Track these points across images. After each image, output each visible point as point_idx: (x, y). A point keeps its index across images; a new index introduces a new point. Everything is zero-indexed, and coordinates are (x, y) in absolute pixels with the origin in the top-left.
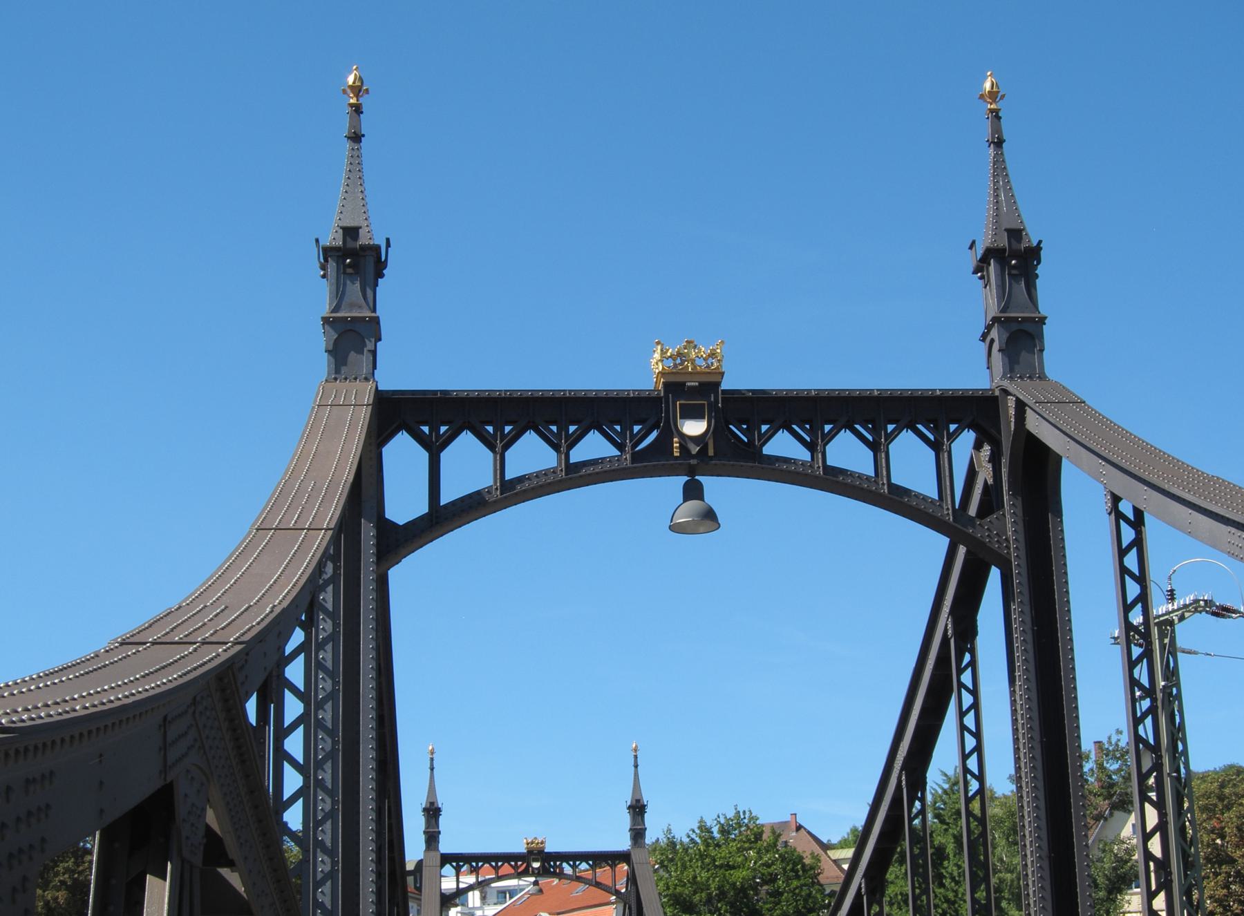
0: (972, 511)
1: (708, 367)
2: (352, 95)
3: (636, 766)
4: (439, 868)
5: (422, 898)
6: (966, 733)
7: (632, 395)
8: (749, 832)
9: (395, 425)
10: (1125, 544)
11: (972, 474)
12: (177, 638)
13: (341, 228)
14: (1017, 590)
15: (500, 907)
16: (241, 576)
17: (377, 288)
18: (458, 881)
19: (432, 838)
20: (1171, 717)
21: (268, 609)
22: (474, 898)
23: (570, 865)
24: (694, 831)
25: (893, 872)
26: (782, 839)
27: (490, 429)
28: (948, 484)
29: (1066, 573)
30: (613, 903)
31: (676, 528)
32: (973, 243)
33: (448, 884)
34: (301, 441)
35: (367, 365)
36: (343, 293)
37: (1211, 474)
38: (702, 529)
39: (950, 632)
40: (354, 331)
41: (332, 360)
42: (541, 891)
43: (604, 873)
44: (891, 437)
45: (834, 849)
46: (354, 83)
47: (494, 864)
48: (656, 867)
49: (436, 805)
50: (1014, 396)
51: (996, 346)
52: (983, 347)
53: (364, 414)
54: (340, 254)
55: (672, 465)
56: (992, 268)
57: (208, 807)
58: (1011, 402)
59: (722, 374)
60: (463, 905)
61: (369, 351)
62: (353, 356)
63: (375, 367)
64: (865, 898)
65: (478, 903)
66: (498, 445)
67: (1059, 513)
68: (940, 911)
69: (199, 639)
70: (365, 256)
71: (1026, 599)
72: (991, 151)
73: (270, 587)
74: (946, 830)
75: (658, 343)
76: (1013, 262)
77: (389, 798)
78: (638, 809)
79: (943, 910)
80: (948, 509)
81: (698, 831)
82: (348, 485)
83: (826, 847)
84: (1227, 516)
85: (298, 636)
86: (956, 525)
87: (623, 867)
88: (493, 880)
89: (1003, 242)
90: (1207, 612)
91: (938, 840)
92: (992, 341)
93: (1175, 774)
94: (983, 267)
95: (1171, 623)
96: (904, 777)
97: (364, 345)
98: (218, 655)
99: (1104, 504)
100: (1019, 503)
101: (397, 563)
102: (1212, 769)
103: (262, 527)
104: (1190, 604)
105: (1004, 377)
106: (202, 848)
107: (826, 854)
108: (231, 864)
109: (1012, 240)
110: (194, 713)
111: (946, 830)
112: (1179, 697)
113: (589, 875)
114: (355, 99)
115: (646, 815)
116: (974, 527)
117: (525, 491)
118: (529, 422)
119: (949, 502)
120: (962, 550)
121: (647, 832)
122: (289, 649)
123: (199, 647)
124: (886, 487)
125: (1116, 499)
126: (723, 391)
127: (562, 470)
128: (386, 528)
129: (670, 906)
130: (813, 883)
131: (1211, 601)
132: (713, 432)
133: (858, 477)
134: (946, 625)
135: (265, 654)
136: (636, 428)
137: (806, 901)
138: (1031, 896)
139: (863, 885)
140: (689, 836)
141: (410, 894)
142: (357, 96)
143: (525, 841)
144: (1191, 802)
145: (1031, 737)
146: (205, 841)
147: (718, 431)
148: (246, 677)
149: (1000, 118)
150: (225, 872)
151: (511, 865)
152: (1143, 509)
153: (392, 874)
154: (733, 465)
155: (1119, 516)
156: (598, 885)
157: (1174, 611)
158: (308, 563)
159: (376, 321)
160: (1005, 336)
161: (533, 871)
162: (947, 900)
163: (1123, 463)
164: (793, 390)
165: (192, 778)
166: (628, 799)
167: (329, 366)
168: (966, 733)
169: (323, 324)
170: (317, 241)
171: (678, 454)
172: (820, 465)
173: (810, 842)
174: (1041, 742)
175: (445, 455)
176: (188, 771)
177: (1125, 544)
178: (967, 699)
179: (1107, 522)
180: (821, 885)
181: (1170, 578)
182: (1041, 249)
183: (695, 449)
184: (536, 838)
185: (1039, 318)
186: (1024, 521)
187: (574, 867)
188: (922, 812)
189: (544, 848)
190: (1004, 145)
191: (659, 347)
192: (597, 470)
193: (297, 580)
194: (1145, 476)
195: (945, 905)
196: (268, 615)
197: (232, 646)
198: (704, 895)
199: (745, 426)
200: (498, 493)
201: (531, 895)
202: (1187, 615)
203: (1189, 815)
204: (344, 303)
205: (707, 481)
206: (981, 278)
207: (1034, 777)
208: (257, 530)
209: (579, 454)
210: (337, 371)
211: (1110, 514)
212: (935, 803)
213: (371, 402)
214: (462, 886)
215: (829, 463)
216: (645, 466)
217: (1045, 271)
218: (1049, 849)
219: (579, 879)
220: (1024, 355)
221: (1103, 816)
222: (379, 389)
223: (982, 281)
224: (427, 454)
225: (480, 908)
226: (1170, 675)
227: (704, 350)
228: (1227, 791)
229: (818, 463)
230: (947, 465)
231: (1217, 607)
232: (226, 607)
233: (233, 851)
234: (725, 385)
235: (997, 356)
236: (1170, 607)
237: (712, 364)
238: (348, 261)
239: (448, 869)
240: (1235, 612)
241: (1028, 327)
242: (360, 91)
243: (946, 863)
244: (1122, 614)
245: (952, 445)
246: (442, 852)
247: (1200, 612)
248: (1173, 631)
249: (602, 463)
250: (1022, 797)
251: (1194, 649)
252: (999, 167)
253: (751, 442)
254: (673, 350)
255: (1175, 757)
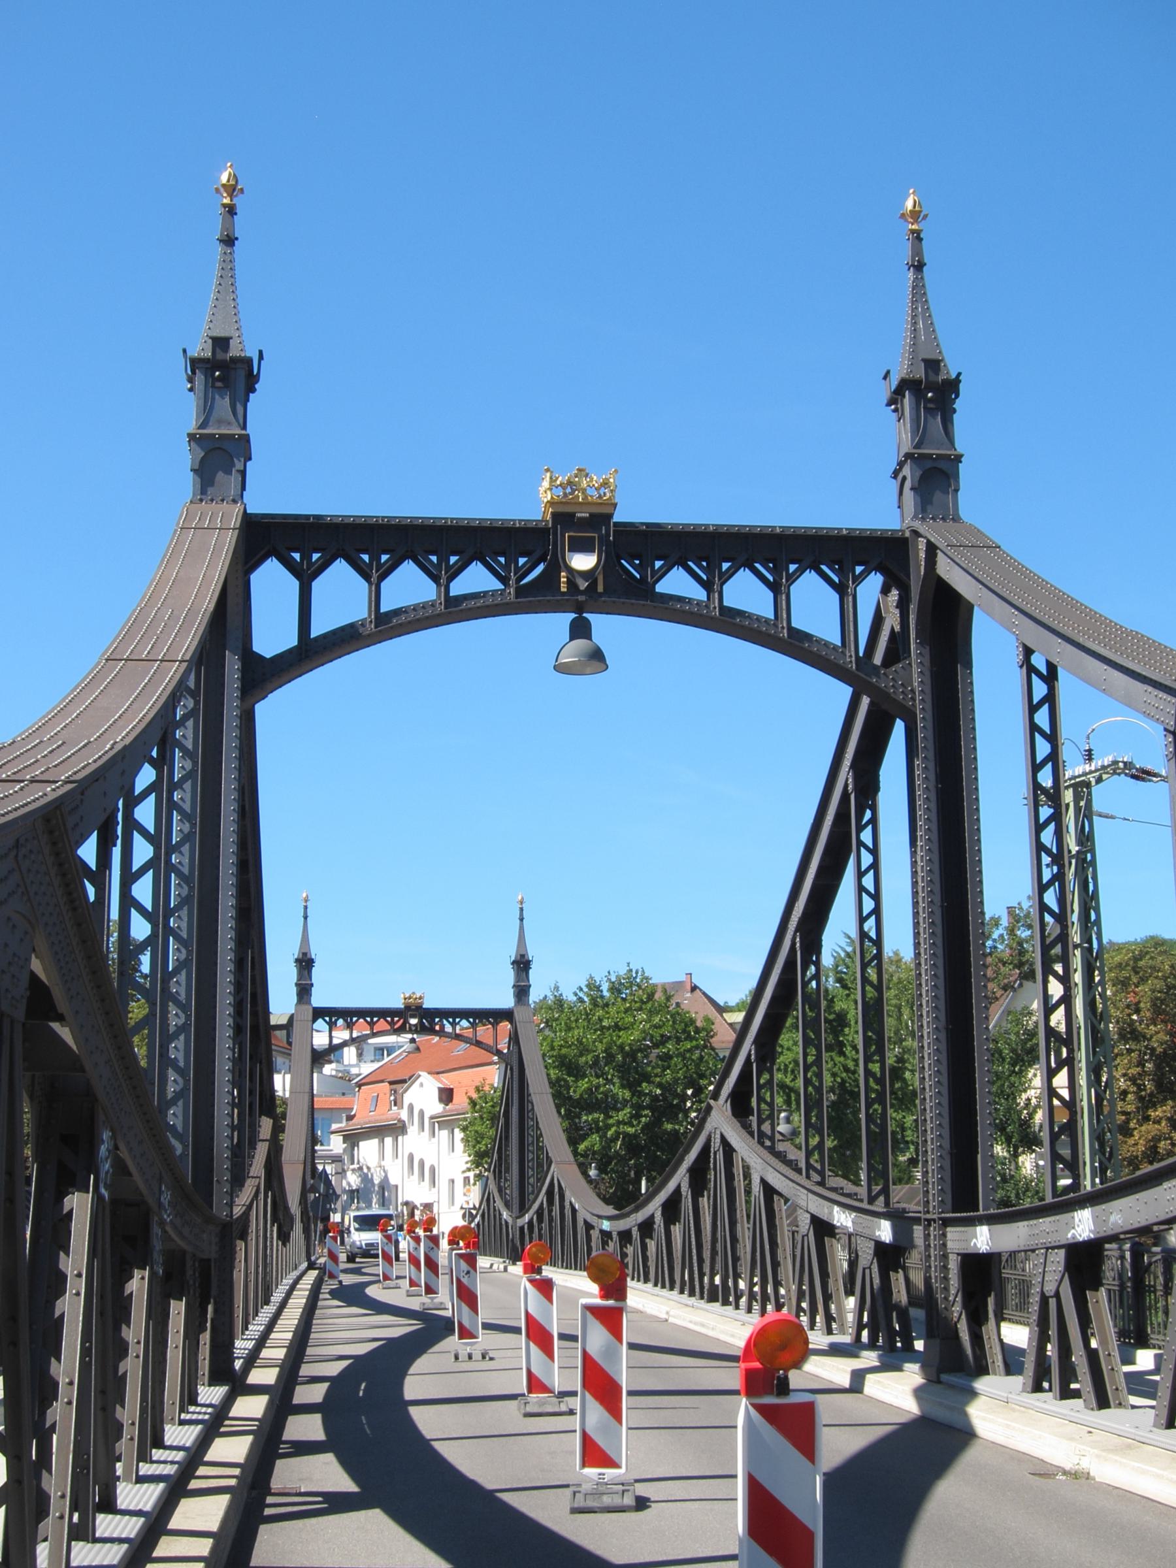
0: (878, 660)
1: (600, 497)
2: (225, 195)
3: (522, 919)
4: (310, 1023)
5: (293, 1052)
6: (864, 894)
7: (518, 525)
8: (641, 991)
9: (262, 552)
10: (1036, 699)
11: (878, 620)
12: (4, 776)
13: (211, 338)
14: (921, 745)
15: (376, 1065)
16: (85, 709)
17: (249, 404)
18: (331, 1037)
19: (304, 991)
20: (1084, 885)
21: (108, 746)
22: (350, 1054)
23: (449, 1022)
24: (581, 989)
25: (785, 1039)
26: (673, 1002)
27: (366, 557)
28: (852, 629)
29: (974, 729)
30: (496, 1063)
31: (560, 668)
32: (888, 372)
33: (320, 1040)
34: (160, 566)
35: (235, 486)
36: (212, 407)
37: (1130, 628)
38: (588, 670)
39: (850, 787)
40: (224, 450)
41: (198, 480)
42: (418, 1049)
43: (484, 1032)
44: (792, 579)
45: (731, 1011)
46: (228, 181)
47: (369, 1019)
48: (542, 1026)
49: (308, 956)
50: (925, 537)
51: (908, 484)
52: (894, 485)
53: (230, 539)
54: (208, 366)
55: (558, 601)
56: (907, 401)
57: (33, 956)
58: (922, 545)
59: (615, 505)
60: (338, 1062)
61: (238, 471)
62: (220, 476)
63: (243, 488)
64: (754, 1065)
65: (354, 1060)
66: (375, 575)
67: (968, 664)
68: (839, 1080)
69: (28, 777)
70: (235, 369)
71: (931, 755)
72: (911, 275)
73: (114, 722)
74: (848, 995)
75: (547, 470)
76: (930, 395)
77: (253, 948)
78: (522, 965)
79: (842, 1078)
80: (851, 656)
81: (585, 989)
82: (208, 615)
83: (721, 1009)
84: (1144, 673)
85: (146, 776)
86: (860, 674)
87: (507, 1026)
88: (367, 1037)
89: (920, 373)
90: (1126, 775)
91: (839, 1006)
92: (904, 478)
93: (1086, 945)
94: (897, 399)
95: (1088, 785)
96: (798, 939)
97: (233, 465)
98: (46, 795)
99: (1016, 656)
100: (927, 651)
101: (263, 699)
102: (1133, 940)
103: (112, 657)
104: (1109, 766)
105: (915, 517)
106: (25, 1001)
107: (722, 1016)
108: (60, 1018)
109: (929, 371)
110: (16, 856)
111: (848, 995)
112: (1093, 863)
113: (469, 1033)
114: (229, 198)
115: (531, 971)
116: (878, 675)
117: (401, 625)
118: (407, 551)
119: (853, 649)
120: (865, 701)
121: (531, 989)
122: (139, 787)
123: (27, 785)
124: (785, 631)
125: (1028, 652)
126: (615, 523)
127: (441, 603)
128: (250, 659)
129: (554, 1068)
130: (705, 1047)
131: (1130, 763)
132: (603, 567)
133: (757, 619)
134: (847, 779)
135: (105, 793)
136: (522, 561)
137: (697, 1066)
138: (927, 1069)
139: (753, 1052)
140: (576, 994)
141: (273, 1047)
142: (231, 196)
143: (402, 996)
144: (1102, 974)
145: (932, 901)
146: (28, 993)
147: (609, 565)
148: (82, 817)
149: (922, 239)
150: (55, 1026)
151: (387, 1021)
152: (1056, 663)
153: (255, 1028)
154: (623, 603)
155: (1031, 670)
156: (478, 1044)
157: (1091, 772)
158: (158, 697)
159: (246, 439)
160: (918, 473)
161: (410, 1028)
162: (847, 1070)
163: (1036, 613)
164: (690, 525)
165: (14, 926)
166: (512, 954)
167: (194, 486)
168: (864, 894)
169: (189, 441)
170: (185, 351)
171: (565, 590)
172: (717, 605)
173: (705, 1003)
174: (942, 906)
175: (316, 585)
176: (9, 919)
177: (1036, 699)
178: (867, 859)
179: (1019, 675)
180: (713, 1049)
181: (1088, 738)
182: (960, 381)
183: (583, 585)
184: (414, 993)
185: (956, 456)
186: (931, 671)
187: (454, 1024)
188: (817, 976)
189: (422, 1003)
190: (925, 269)
191: (548, 475)
192: (478, 605)
193: (144, 715)
194: (1060, 627)
195: (844, 1075)
196: (106, 752)
197: (62, 786)
198: (589, 1057)
199: (637, 562)
200: (373, 626)
201: (409, 1053)
202: (1105, 776)
203: (1100, 989)
204: (212, 419)
205: (597, 621)
206: (896, 410)
207: (934, 943)
208: (107, 660)
209: (458, 587)
210: (203, 492)
211: (1021, 667)
212: (837, 966)
213: (238, 525)
214: (336, 1041)
215: (726, 603)
216: (530, 602)
217: (962, 405)
218: (947, 1021)
219: (458, 1037)
220: (938, 496)
221: (1013, 987)
222: (248, 512)
223: (895, 415)
224: (297, 583)
225: (357, 1065)
226: (1084, 840)
227: (596, 480)
228: (1141, 963)
229: (714, 603)
230: (851, 609)
231: (1137, 769)
232: (64, 743)
233: (62, 1005)
234: (618, 517)
235: (908, 495)
236: (1087, 768)
237: (605, 494)
238: (217, 373)
239: (320, 1024)
240: (1155, 775)
241: (942, 465)
242: (234, 190)
243: (847, 1030)
244: (1031, 774)
245: (858, 589)
246: (314, 1006)
247: (1119, 774)
248: (1090, 794)
249: (484, 597)
250: (919, 964)
251: (1110, 813)
252: (919, 292)
253: (643, 579)
254: (563, 478)
255: (1087, 926)
